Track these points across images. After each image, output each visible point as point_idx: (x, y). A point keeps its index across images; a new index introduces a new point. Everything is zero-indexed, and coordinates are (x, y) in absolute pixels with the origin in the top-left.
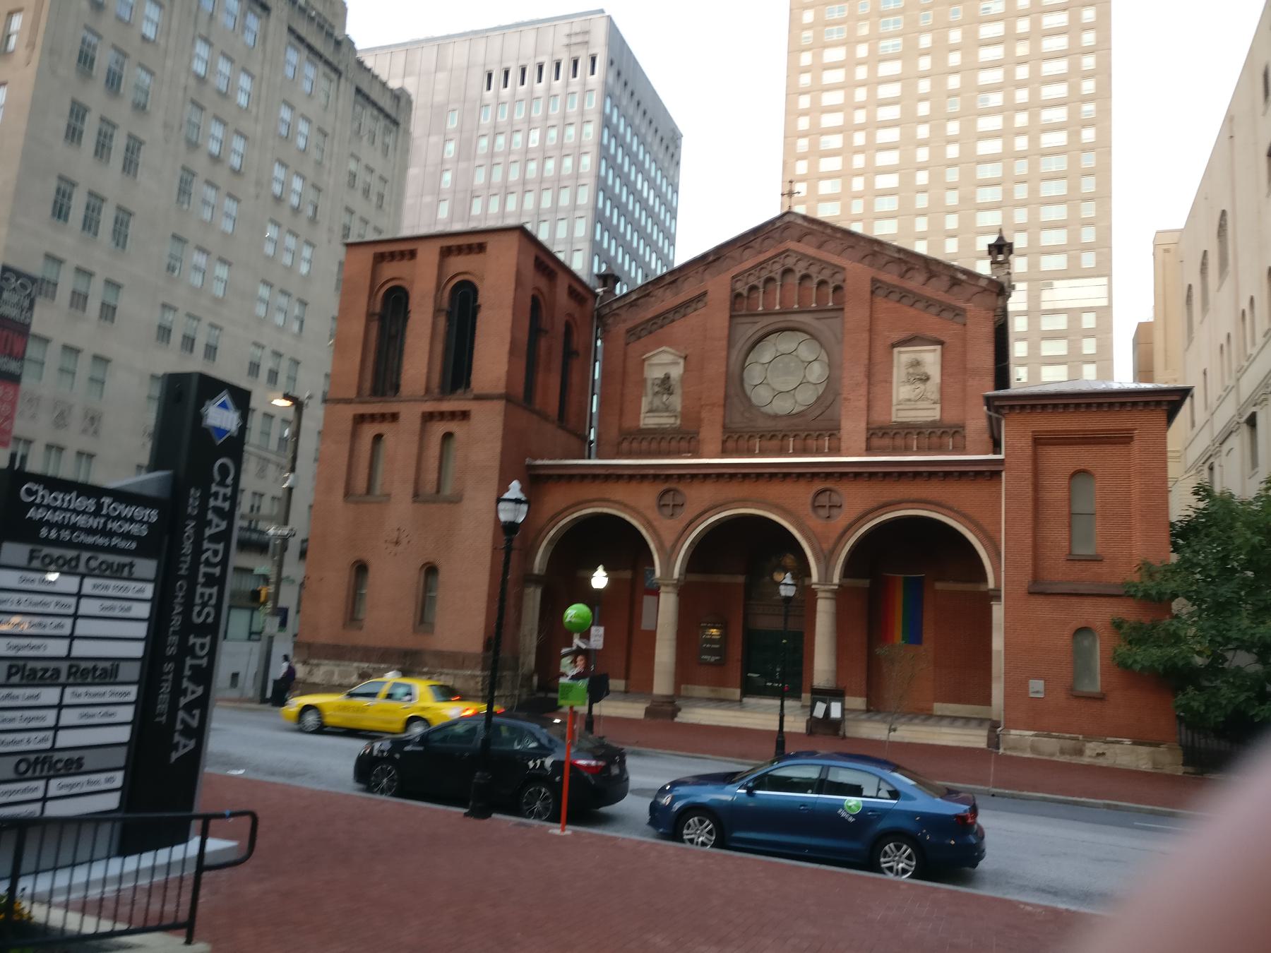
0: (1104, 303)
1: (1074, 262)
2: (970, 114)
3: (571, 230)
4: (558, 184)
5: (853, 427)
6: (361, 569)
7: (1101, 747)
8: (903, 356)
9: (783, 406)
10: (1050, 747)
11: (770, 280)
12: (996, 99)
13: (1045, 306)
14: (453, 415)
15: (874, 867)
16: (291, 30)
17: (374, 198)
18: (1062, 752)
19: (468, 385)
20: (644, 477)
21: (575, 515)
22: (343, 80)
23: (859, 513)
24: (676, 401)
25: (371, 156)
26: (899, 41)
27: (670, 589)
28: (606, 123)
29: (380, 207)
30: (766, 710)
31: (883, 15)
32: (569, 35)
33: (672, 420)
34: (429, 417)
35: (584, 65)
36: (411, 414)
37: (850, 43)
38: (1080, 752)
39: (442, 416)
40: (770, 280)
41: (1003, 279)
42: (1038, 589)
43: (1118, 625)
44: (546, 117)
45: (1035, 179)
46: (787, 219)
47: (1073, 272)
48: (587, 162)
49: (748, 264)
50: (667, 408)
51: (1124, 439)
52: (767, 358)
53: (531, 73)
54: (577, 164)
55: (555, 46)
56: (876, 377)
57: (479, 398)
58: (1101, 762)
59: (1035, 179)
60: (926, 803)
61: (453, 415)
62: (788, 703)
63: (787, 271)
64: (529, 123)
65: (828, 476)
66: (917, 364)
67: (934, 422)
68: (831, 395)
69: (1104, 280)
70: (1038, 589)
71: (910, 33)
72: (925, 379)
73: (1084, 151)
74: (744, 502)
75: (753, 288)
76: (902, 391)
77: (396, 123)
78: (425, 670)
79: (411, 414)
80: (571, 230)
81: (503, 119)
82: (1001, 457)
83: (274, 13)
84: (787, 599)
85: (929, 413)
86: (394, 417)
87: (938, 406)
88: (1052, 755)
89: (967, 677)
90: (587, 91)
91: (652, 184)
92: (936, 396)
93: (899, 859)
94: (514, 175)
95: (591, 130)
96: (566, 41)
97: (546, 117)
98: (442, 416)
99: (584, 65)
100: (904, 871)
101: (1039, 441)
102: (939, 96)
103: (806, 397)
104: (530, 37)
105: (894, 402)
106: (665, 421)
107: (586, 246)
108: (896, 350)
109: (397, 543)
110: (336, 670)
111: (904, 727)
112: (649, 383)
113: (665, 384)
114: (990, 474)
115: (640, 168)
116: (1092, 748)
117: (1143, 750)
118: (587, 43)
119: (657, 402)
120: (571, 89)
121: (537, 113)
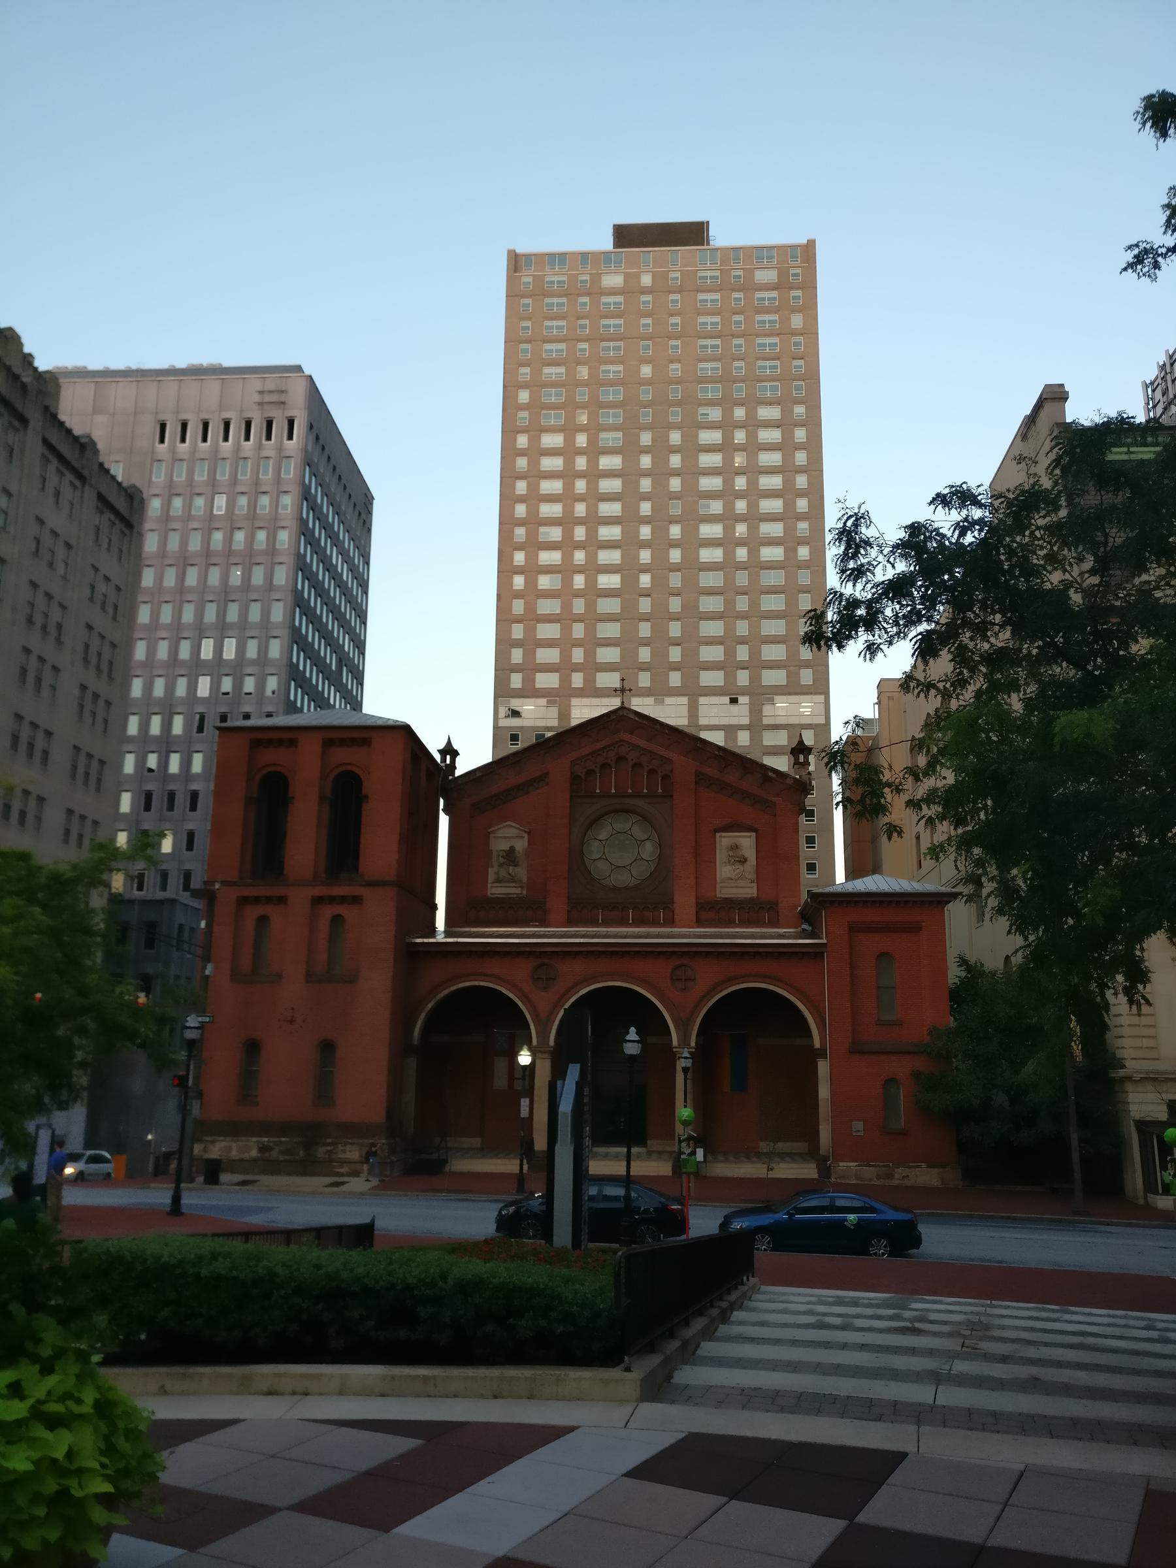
0: (822, 720)
1: (793, 677)
2: (691, 520)
3: (266, 613)
4: (249, 559)
5: (684, 902)
6: (253, 1048)
7: (906, 1172)
8: (724, 840)
9: (623, 879)
10: (869, 1173)
11: (605, 766)
12: (716, 507)
13: (766, 721)
14: (343, 900)
15: (867, 1253)
16: (45, 441)
17: (110, 610)
18: (878, 1177)
19: (355, 867)
20: (519, 954)
21: (453, 988)
22: (87, 488)
23: (710, 988)
24: (521, 872)
25: (109, 565)
26: (620, 435)
27: (546, 1056)
28: (306, 495)
29: (115, 618)
30: (616, 1157)
31: (603, 405)
32: (261, 392)
33: (518, 891)
34: (318, 901)
35: (279, 428)
36: (299, 898)
37: (569, 430)
38: (891, 1176)
39: (332, 900)
40: (605, 766)
41: (805, 778)
42: (858, 1049)
43: (916, 1075)
44: (234, 481)
45: (755, 591)
46: (620, 713)
47: (792, 689)
48: (284, 536)
49: (586, 750)
50: (512, 879)
51: (914, 929)
52: (603, 836)
53: (215, 430)
54: (272, 538)
55: (245, 401)
56: (703, 857)
57: (372, 884)
58: (907, 1182)
59: (755, 591)
60: (892, 1215)
61: (343, 900)
62: (635, 1150)
63: (621, 759)
64: (214, 487)
65: (683, 954)
66: (735, 847)
67: (752, 899)
68: (662, 869)
69: (821, 698)
70: (858, 1049)
71: (630, 428)
72: (743, 861)
73: (800, 568)
74: (611, 976)
75: (590, 772)
76: (724, 871)
77: (129, 525)
78: (329, 1141)
79: (299, 898)
80: (266, 613)
81: (180, 477)
82: (824, 941)
83: (32, 424)
84: (632, 1058)
85: (749, 891)
86: (281, 900)
87: (755, 885)
88: (871, 1180)
89: (795, 1120)
90: (282, 457)
91: (343, 552)
92: (753, 876)
93: (881, 1248)
94: (195, 544)
95: (288, 501)
96: (256, 398)
97: (234, 481)
98: (332, 900)
99: (279, 428)
100: (883, 1254)
101: (854, 929)
102: (660, 496)
103: (640, 872)
104: (213, 388)
105: (718, 880)
106: (512, 890)
107: (284, 633)
108: (718, 835)
109: (292, 1021)
110: (234, 1145)
111: (782, 1165)
112: (495, 854)
113: (510, 856)
114: (814, 954)
115: (336, 542)
116: (900, 1172)
117: (936, 1171)
118: (283, 403)
119: (503, 873)
120: (265, 453)
121: (223, 476)
